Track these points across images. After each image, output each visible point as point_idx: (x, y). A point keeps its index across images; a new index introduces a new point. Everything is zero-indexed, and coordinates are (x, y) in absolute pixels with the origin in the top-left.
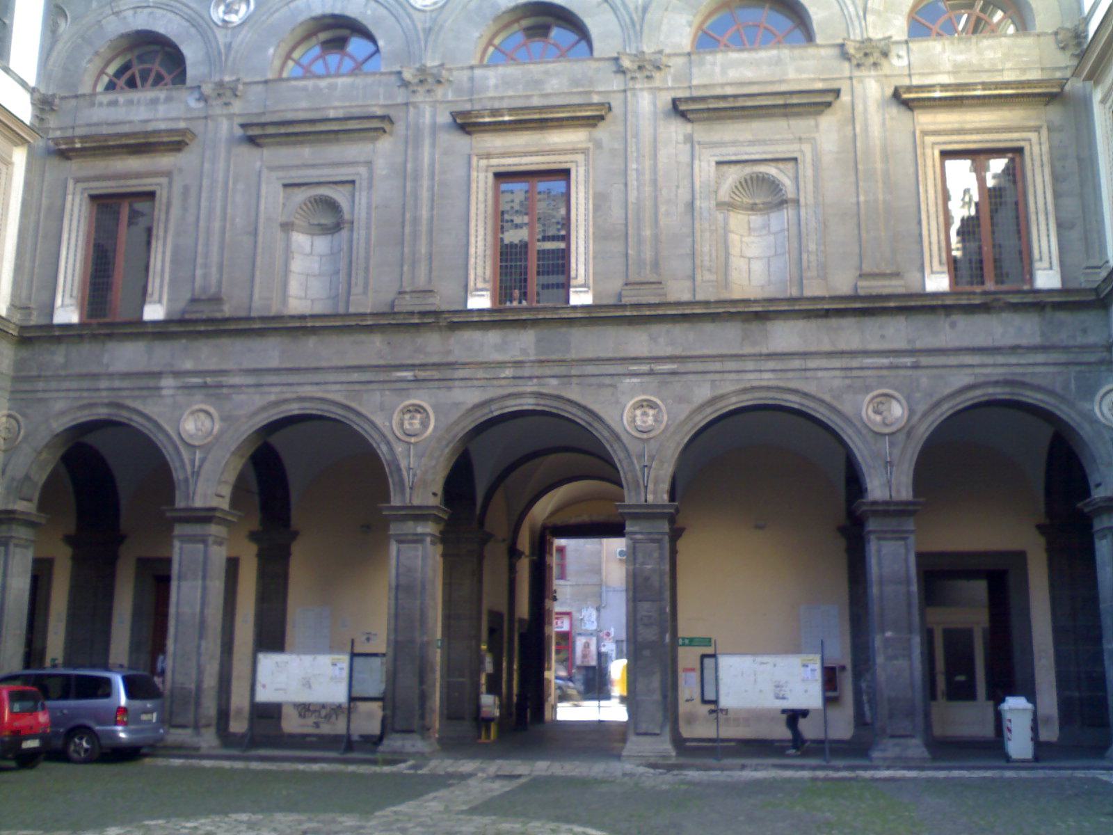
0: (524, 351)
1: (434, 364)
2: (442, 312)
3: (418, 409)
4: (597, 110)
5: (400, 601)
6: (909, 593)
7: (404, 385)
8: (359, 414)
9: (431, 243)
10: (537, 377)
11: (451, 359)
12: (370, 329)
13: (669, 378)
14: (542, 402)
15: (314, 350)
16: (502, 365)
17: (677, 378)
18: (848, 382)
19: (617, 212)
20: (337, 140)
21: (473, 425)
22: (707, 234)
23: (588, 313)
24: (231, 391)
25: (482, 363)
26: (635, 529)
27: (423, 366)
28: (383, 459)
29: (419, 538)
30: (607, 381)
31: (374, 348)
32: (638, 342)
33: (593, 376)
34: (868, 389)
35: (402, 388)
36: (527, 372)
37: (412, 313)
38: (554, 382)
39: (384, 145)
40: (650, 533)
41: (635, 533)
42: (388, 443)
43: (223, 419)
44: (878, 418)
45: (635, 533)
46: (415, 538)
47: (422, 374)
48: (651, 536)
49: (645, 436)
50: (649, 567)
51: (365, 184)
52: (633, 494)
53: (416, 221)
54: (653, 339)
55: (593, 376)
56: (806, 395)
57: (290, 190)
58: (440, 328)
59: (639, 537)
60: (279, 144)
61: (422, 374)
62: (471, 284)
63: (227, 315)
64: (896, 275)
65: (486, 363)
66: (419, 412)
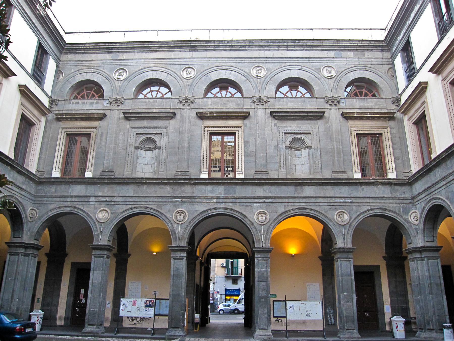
0: (220, 193)
3: (182, 212)
7: (178, 203)
10: (225, 202)
11: (194, 195)
13: (270, 204)
15: (145, 190)
16: (212, 197)
17: (273, 204)
18: (330, 207)
24: (115, 203)
26: (259, 256)
27: (184, 197)
30: (249, 204)
31: (167, 190)
32: (260, 191)
35: (176, 205)
36: (221, 200)
37: (181, 179)
38: (230, 204)
39: (172, 122)
42: (171, 224)
43: (112, 213)
44: (340, 219)
47: (184, 200)
51: (165, 134)
57: (138, 135)
58: (191, 184)
60: (136, 120)
61: (184, 200)
64: (344, 172)
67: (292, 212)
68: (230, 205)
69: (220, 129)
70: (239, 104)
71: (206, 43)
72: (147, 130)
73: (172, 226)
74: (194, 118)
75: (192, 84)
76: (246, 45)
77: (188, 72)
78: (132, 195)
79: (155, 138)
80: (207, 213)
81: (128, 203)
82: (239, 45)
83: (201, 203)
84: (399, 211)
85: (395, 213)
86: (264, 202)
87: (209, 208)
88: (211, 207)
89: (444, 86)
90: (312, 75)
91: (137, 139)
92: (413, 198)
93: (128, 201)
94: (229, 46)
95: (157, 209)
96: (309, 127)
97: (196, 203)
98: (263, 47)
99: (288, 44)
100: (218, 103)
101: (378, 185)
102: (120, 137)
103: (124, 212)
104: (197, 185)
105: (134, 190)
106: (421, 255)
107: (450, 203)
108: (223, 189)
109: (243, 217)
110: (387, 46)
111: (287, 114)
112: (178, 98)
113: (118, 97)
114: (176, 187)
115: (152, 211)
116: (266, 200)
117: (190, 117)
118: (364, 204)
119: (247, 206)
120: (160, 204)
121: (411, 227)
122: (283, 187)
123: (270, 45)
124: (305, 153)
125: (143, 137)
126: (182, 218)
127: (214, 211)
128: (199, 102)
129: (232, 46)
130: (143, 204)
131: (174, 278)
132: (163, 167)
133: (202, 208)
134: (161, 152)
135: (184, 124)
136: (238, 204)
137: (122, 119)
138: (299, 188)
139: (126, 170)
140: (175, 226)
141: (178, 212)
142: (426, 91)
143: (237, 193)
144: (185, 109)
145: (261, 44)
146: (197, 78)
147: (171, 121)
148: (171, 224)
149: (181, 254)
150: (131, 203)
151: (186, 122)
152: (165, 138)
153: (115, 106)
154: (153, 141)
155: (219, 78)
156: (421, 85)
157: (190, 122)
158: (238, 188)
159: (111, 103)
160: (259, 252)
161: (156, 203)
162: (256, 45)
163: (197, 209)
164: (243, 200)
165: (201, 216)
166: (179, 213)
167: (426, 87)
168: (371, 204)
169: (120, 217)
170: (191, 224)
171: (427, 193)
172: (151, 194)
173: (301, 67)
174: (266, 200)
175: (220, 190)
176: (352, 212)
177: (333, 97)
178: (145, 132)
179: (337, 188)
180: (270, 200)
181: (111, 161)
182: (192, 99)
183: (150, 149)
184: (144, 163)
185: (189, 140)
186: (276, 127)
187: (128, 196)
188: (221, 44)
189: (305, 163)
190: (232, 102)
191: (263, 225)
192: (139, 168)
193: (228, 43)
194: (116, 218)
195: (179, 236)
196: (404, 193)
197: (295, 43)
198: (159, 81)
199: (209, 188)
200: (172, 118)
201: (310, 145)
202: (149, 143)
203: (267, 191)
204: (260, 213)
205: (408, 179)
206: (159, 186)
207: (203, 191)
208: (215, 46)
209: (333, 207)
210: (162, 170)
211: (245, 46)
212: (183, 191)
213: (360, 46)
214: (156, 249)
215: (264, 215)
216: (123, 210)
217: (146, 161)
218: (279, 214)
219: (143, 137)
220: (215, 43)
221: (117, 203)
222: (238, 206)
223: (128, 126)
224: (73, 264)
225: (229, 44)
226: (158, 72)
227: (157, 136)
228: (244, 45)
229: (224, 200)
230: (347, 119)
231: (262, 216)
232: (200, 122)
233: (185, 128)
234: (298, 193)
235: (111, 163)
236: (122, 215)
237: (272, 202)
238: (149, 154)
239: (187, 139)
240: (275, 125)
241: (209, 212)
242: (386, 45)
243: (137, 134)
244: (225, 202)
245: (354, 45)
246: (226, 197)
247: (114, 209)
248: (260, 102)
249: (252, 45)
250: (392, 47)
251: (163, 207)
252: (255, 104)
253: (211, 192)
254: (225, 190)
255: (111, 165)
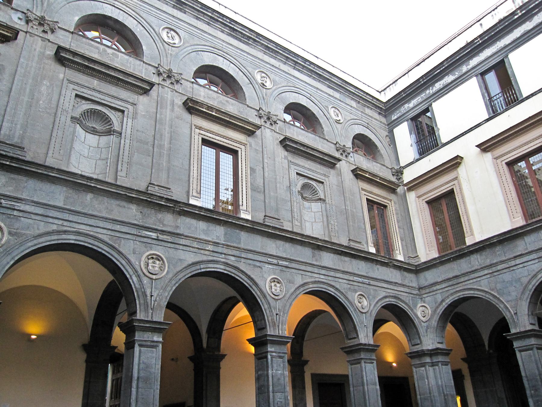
0: (218, 237)
1: (169, 232)
2: (180, 202)
3: (159, 258)
4: (254, 128)
5: (140, 390)
6: (377, 390)
7: (149, 241)
8: (120, 253)
9: (169, 161)
10: (225, 254)
11: (178, 231)
12: (131, 200)
13: (284, 269)
14: (228, 269)
15: (88, 202)
16: (207, 242)
17: (288, 270)
18: (349, 286)
19: (259, 181)
20: (117, 85)
21: (438, 317)
22: (295, 203)
23: (253, 225)
24: (21, 214)
25: (197, 239)
26: (273, 349)
27: (163, 232)
28: (133, 286)
29: (155, 344)
30: (258, 264)
31: (132, 213)
32: (273, 247)
33: (252, 260)
34: (356, 291)
35: (147, 243)
36: (220, 250)
37: (162, 198)
38: (233, 258)
39: (143, 100)
40: (280, 353)
41: (272, 352)
42: (138, 276)
43: (10, 233)
44: (360, 305)
45: (272, 352)
46: (152, 344)
47: (161, 237)
48: (280, 354)
49: (276, 298)
50: (280, 372)
51: (131, 115)
52: (272, 329)
53: (161, 146)
54: (278, 247)
55: (252, 260)
56: (337, 289)
57: (79, 100)
58: (174, 212)
59: (274, 354)
60: (79, 71)
61: (161, 237)
62: (191, 193)
63: (28, 159)
64: (360, 243)
65: (199, 239)
66: (159, 260)
67: (311, 286)
68: (232, 260)
69: (217, 138)
70: (241, 112)
71: (201, 8)
72: (97, 96)
73: (140, 281)
74: (179, 107)
75: (177, 54)
76: (251, 38)
77: (169, 35)
78: (61, 204)
79: (113, 116)
80: (198, 267)
81: (51, 220)
82: (241, 33)
83: (188, 249)
84: (409, 302)
85: (406, 304)
86: (277, 265)
87: (201, 259)
88: (205, 258)
89: (496, 166)
90: (320, 111)
91: (76, 106)
92: (420, 288)
93: (51, 215)
94: (230, 27)
95: (111, 243)
96: (321, 174)
97: (181, 247)
98: (269, 51)
99: (299, 61)
100: (214, 99)
101: (390, 267)
102: (43, 89)
103: (40, 236)
104: (184, 215)
105: (67, 198)
106: (431, 360)
107: (499, 294)
108: (223, 233)
109: (251, 284)
110: (386, 111)
111: (302, 148)
112: (157, 68)
113: (47, 18)
114: (147, 211)
115: (101, 245)
116: (281, 262)
117: (173, 104)
118: (380, 289)
119: (255, 266)
120: (118, 235)
121: (421, 325)
122: (299, 248)
123: (278, 52)
124: (316, 206)
125: (86, 106)
126: (157, 269)
127: (210, 265)
128: (187, 87)
129: (234, 30)
130: (83, 228)
131: (140, 385)
132: (125, 169)
133: (190, 258)
134: (122, 142)
135: (164, 111)
136: (243, 260)
137: (48, 58)
138: (316, 252)
139: (50, 154)
140: (145, 281)
141: (152, 257)
142: (458, 167)
143: (242, 244)
144: (166, 88)
145: (269, 46)
146: (185, 50)
147: (141, 97)
148: (138, 276)
149: (153, 337)
150: (56, 221)
151: (166, 108)
152: (130, 121)
153: (37, 30)
154: (106, 119)
155: (214, 64)
156: (457, 159)
157: (172, 110)
158: (244, 235)
159: (27, 22)
160: (274, 343)
161: (109, 233)
162: (263, 44)
163: (182, 257)
164: (250, 256)
165: (189, 271)
166: (153, 258)
167: (460, 163)
168: (389, 291)
169: (30, 244)
170: (174, 282)
171: (451, 283)
172: (100, 211)
173: (309, 95)
174: (281, 262)
175: (218, 233)
176: (371, 297)
177: (344, 146)
178: (94, 98)
179: (355, 262)
180: (285, 263)
181: (19, 126)
182: (177, 77)
183: (94, 131)
184: (82, 153)
185: (171, 139)
186: (286, 161)
187: (54, 207)
188: (220, 20)
189: (317, 221)
190: (232, 105)
191: (278, 300)
192: (73, 159)
193: (230, 23)
194: (21, 244)
195: (152, 302)
196: (411, 281)
197: (305, 63)
198: (118, 27)
199: (202, 225)
200: (146, 92)
201: (322, 197)
202: (97, 119)
203: (281, 249)
204: (274, 280)
205: (416, 266)
206: (118, 202)
207: (193, 229)
208: (211, 17)
209: (352, 287)
210: (123, 174)
211: (249, 38)
212: (161, 221)
213: (363, 99)
214: (34, 328)
215: (278, 285)
216: (37, 232)
217: (86, 151)
218: (297, 286)
219: (86, 106)
220: (212, 14)
221: (26, 215)
222: (244, 265)
223: (61, 76)
224: (314, 376)
225: (230, 25)
226: (122, 12)
227: (113, 112)
228: (248, 36)
229: (225, 251)
230: (357, 178)
231: (275, 285)
232: (187, 116)
233: (166, 116)
234: (316, 260)
235: (18, 132)
236: (35, 242)
237: (287, 267)
238: (92, 139)
239: (167, 136)
240: (286, 158)
241: (202, 266)
242: (388, 109)
243: (77, 96)
244: (225, 254)
245: (358, 96)
246: (228, 246)
247: (17, 225)
248: (269, 119)
249: (258, 42)
250: (392, 113)
251: (123, 241)
252: (263, 120)
253: (206, 232)
254: (226, 234)
255: (17, 134)
